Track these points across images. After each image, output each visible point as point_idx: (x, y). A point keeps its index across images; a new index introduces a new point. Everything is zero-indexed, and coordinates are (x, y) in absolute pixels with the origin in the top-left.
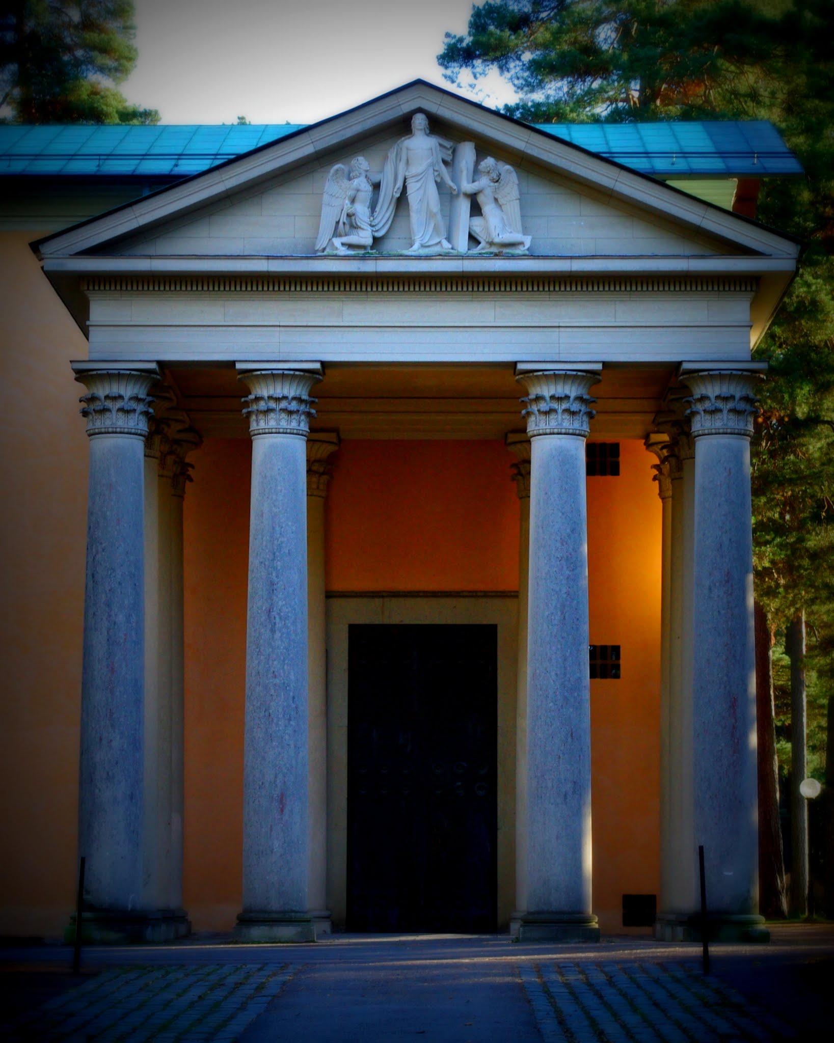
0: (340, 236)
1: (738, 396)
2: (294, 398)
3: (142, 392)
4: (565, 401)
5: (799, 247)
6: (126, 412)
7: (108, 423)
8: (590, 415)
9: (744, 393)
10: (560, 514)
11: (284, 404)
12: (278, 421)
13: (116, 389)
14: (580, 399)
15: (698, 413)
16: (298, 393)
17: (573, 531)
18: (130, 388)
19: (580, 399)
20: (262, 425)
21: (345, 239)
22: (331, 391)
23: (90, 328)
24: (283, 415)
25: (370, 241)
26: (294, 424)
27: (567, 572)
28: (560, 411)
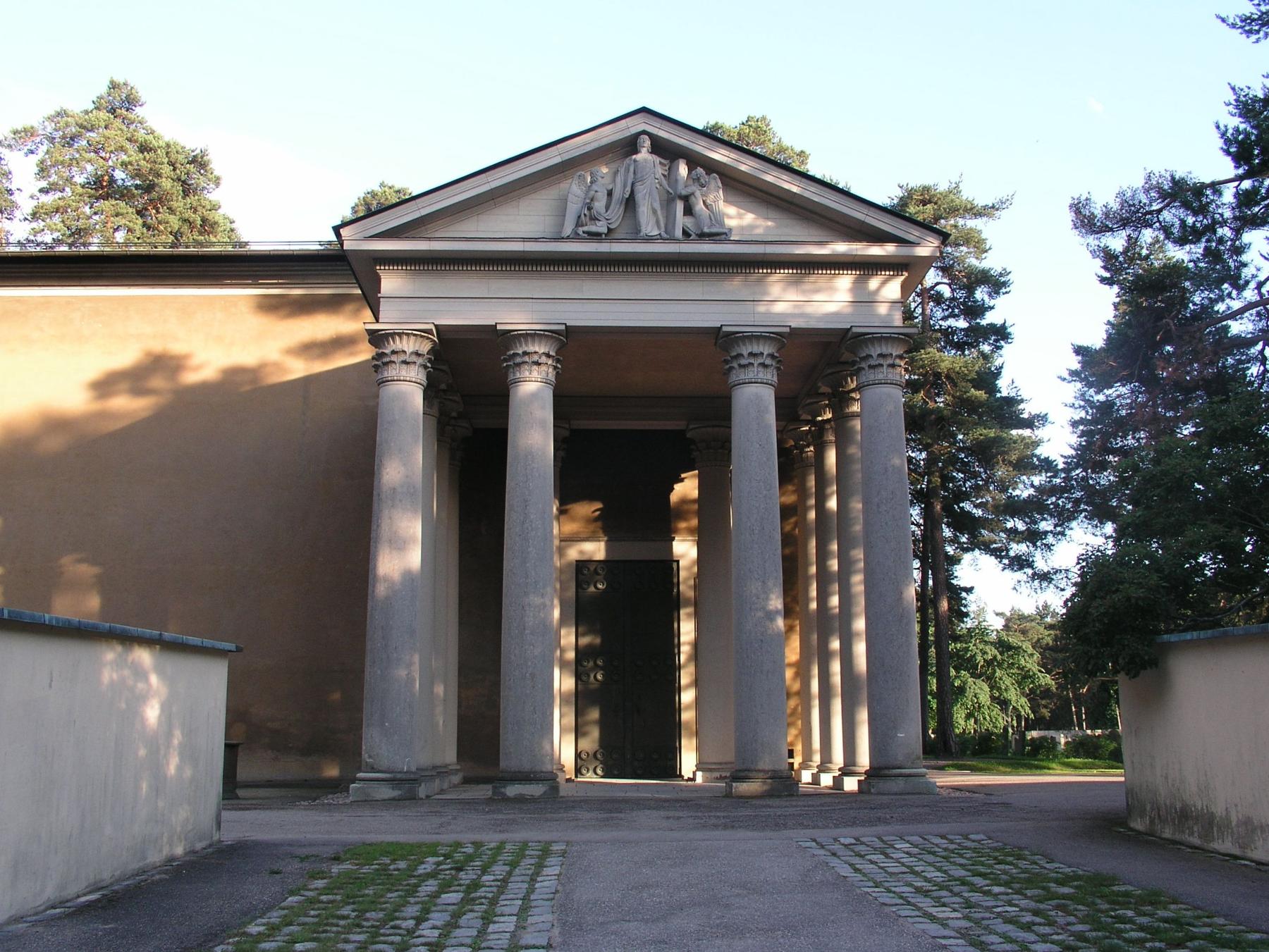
6: (764, 365)
7: (751, 375)
8: (778, 369)
14: (772, 356)
19: (772, 356)
21: (586, 229)
22: (572, 344)
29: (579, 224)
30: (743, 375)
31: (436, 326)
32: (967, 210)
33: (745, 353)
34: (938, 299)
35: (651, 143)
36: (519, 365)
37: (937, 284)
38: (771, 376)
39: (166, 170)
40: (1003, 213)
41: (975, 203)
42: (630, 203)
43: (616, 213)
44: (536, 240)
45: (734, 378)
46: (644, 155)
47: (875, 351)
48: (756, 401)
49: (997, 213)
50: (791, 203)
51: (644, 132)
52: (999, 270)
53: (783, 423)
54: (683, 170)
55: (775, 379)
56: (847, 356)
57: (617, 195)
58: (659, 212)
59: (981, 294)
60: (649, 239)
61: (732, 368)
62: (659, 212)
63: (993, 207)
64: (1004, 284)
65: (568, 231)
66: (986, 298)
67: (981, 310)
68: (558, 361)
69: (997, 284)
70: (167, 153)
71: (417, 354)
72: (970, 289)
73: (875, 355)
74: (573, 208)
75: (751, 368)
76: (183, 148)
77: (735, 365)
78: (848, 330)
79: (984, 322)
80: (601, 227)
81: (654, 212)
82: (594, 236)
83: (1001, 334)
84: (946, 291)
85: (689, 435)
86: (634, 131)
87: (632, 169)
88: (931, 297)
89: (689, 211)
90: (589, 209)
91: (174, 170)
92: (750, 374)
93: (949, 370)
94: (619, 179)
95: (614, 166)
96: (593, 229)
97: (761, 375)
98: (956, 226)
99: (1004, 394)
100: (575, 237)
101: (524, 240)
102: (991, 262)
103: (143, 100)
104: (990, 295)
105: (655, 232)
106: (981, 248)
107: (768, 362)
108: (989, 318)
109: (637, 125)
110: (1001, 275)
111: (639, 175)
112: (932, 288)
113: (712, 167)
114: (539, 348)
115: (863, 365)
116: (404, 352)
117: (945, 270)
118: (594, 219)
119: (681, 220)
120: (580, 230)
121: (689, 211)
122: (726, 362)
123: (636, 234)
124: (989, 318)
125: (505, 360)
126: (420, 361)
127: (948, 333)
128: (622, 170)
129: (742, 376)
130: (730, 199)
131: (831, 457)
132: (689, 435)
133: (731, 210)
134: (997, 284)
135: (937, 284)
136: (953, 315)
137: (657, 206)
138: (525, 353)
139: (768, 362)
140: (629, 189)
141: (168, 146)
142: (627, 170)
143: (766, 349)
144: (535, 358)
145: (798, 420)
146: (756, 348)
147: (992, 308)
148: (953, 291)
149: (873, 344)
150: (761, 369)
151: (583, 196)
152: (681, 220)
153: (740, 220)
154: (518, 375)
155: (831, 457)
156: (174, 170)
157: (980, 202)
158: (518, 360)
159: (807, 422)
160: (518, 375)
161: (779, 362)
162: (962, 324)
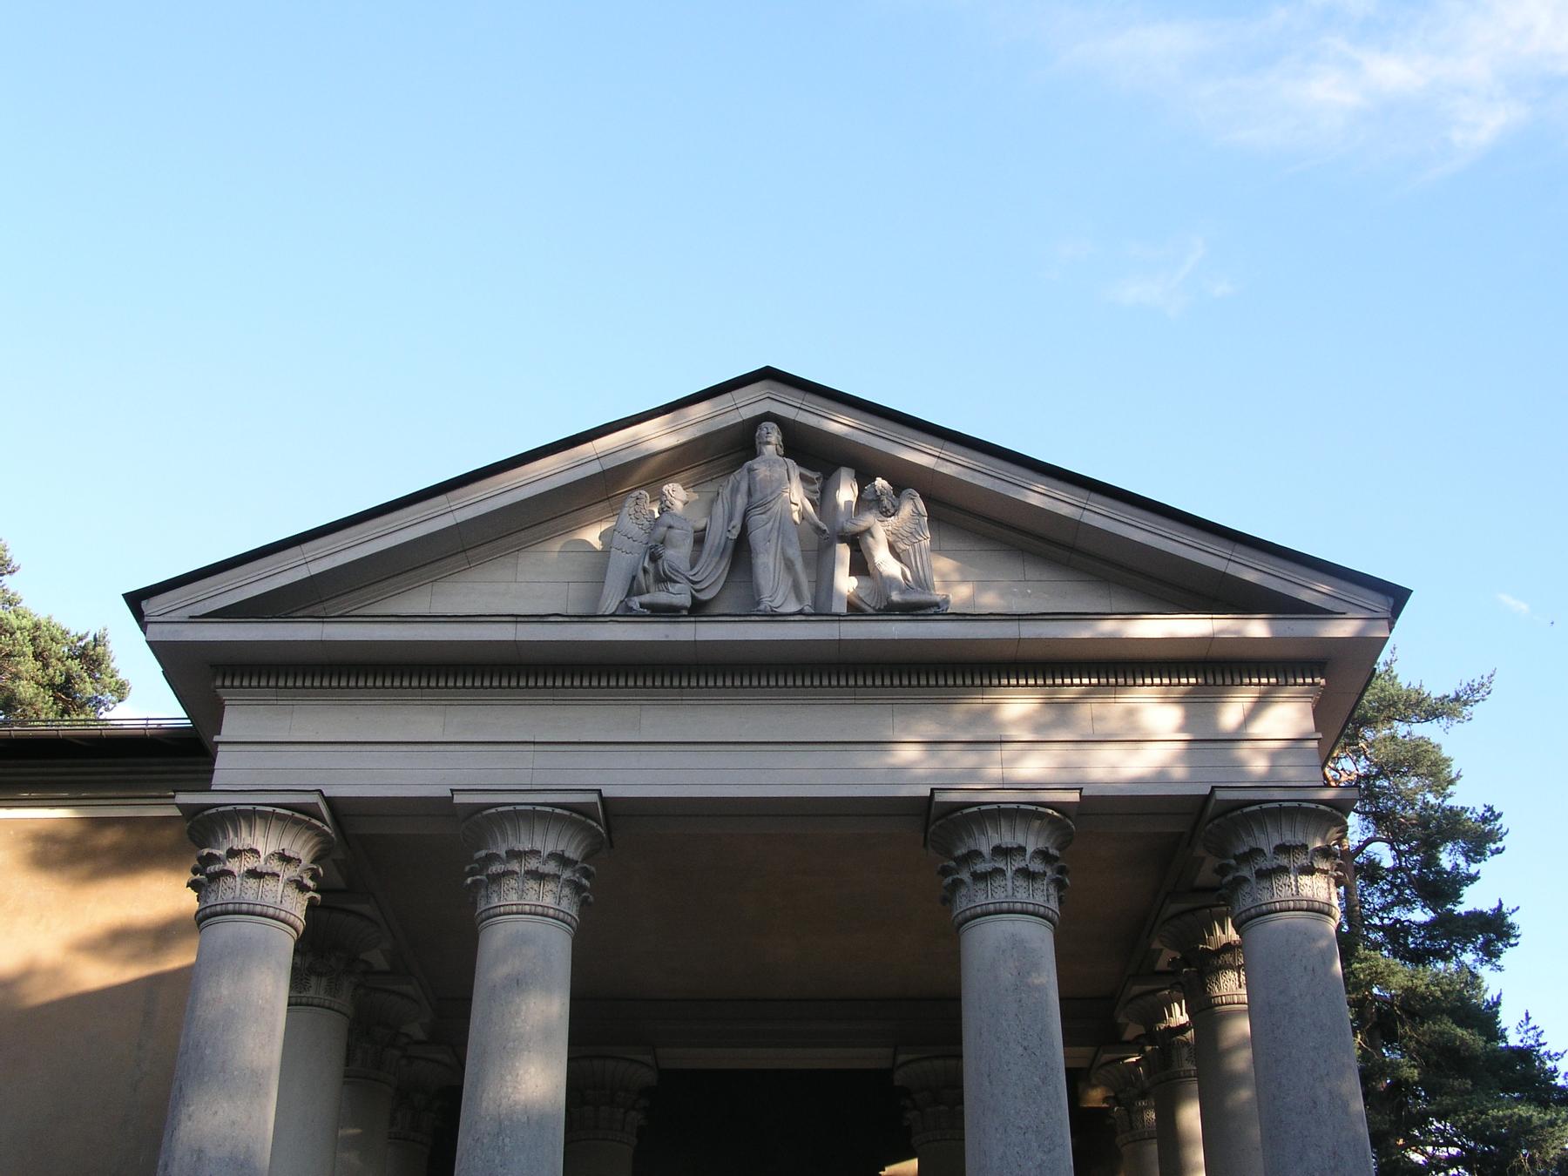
0: (640, 593)
1: (1030, 850)
2: (552, 856)
3: (301, 848)
4: (1019, 858)
5: (1391, 601)
6: (1028, 875)
7: (1000, 895)
8: (1060, 885)
9: (1041, 845)
10: (1020, 1050)
11: (533, 864)
12: (522, 893)
13: (1006, 837)
14: (1043, 854)
15: (1245, 880)
16: (560, 848)
17: (1044, 1080)
18: (552, 836)
19: (1043, 854)
20: (513, 898)
21: (646, 598)
22: (618, 840)
23: (220, 748)
24: (532, 884)
25: (687, 602)
26: (549, 900)
27: (1039, 1156)
28: (1009, 874)
29: (633, 589)
30: (981, 897)
31: (329, 801)
32: (1409, 704)
33: (986, 849)
34: (1372, 872)
35: (779, 428)
36: (497, 878)
37: (1369, 842)
38: (1043, 896)
39: (29, 665)
40: (1475, 710)
41: (1426, 690)
42: (741, 551)
43: (712, 574)
44: (541, 618)
45: (962, 904)
46: (771, 462)
47: (1268, 840)
48: (1014, 958)
49: (1466, 711)
50: (1072, 549)
51: (768, 417)
52: (1480, 810)
53: (1087, 1051)
54: (846, 493)
55: (1054, 905)
56: (1206, 876)
57: (714, 539)
58: (799, 566)
59: (1447, 858)
60: (774, 616)
61: (958, 883)
62: (799, 566)
63: (1457, 699)
64: (1493, 836)
65: (610, 604)
66: (1461, 861)
67: (1451, 886)
68: (586, 874)
69: (1480, 837)
70: (33, 639)
71: (284, 858)
72: (1430, 847)
73: (1268, 849)
74: (623, 563)
75: (999, 882)
76: (65, 633)
77: (965, 876)
78: (1206, 799)
79: (1460, 909)
80: (679, 595)
81: (789, 565)
82: (667, 612)
83: (1493, 930)
84: (1383, 854)
85: (899, 1078)
86: (747, 413)
87: (744, 487)
88: (1359, 869)
89: (861, 566)
90: (654, 558)
91: (46, 666)
92: (1001, 892)
93: (1407, 990)
94: (720, 510)
95: (711, 488)
96: (660, 597)
97: (1022, 895)
98: (1393, 738)
99: (1514, 1040)
100: (625, 613)
101: (517, 619)
102: (1466, 797)
103: (15, 563)
104: (1466, 854)
105: (792, 607)
106: (1437, 773)
107: (1037, 866)
108: (1472, 900)
109: (748, 404)
110: (1485, 820)
111: (757, 496)
112: (1360, 849)
113: (905, 479)
114: (548, 842)
115: (1246, 872)
116: (255, 852)
117: (1381, 819)
118: (663, 579)
119: (846, 583)
120: (635, 603)
121: (861, 566)
122: (945, 872)
123: (753, 610)
124: (1472, 900)
125: (472, 873)
126: (291, 872)
127: (1396, 933)
128: (726, 492)
129: (981, 899)
130: (947, 545)
131: (1191, 1116)
132: (899, 1078)
133: (944, 565)
134: (1480, 837)
135: (1369, 842)
136: (1402, 902)
137: (795, 553)
138: (514, 855)
139: (1037, 866)
140: (737, 522)
141: (37, 627)
142: (735, 491)
143: (1032, 841)
144: (533, 864)
145: (1111, 1038)
146: (1007, 838)
147: (1473, 878)
148: (1400, 854)
149: (1263, 828)
150: (1020, 882)
151: (644, 538)
152: (846, 583)
153: (968, 588)
154: (495, 901)
155: (1191, 1116)
156: (46, 666)
157: (1437, 688)
158: (496, 868)
159: (1136, 1045)
160: (495, 901)
161: (1061, 870)
162: (1420, 915)
